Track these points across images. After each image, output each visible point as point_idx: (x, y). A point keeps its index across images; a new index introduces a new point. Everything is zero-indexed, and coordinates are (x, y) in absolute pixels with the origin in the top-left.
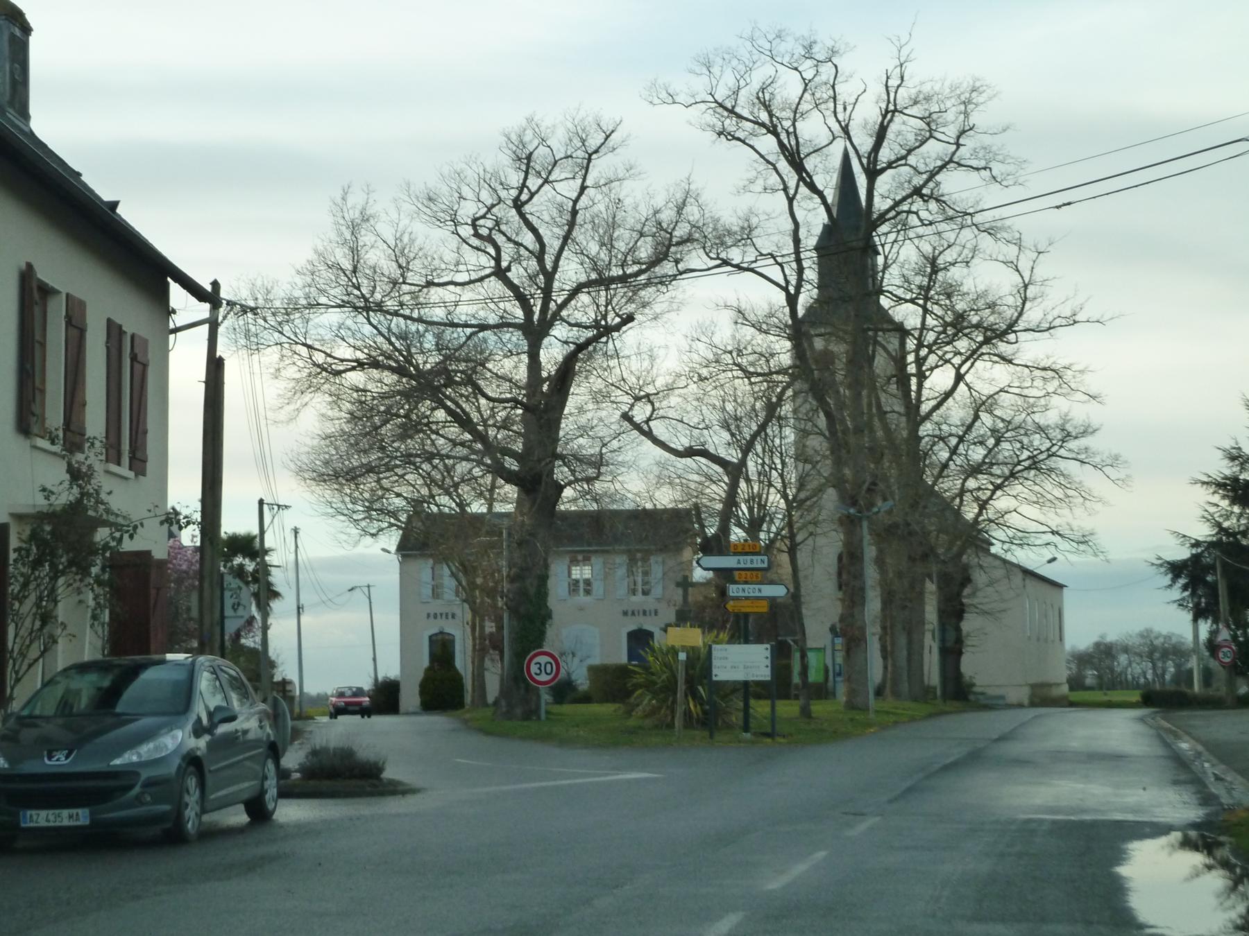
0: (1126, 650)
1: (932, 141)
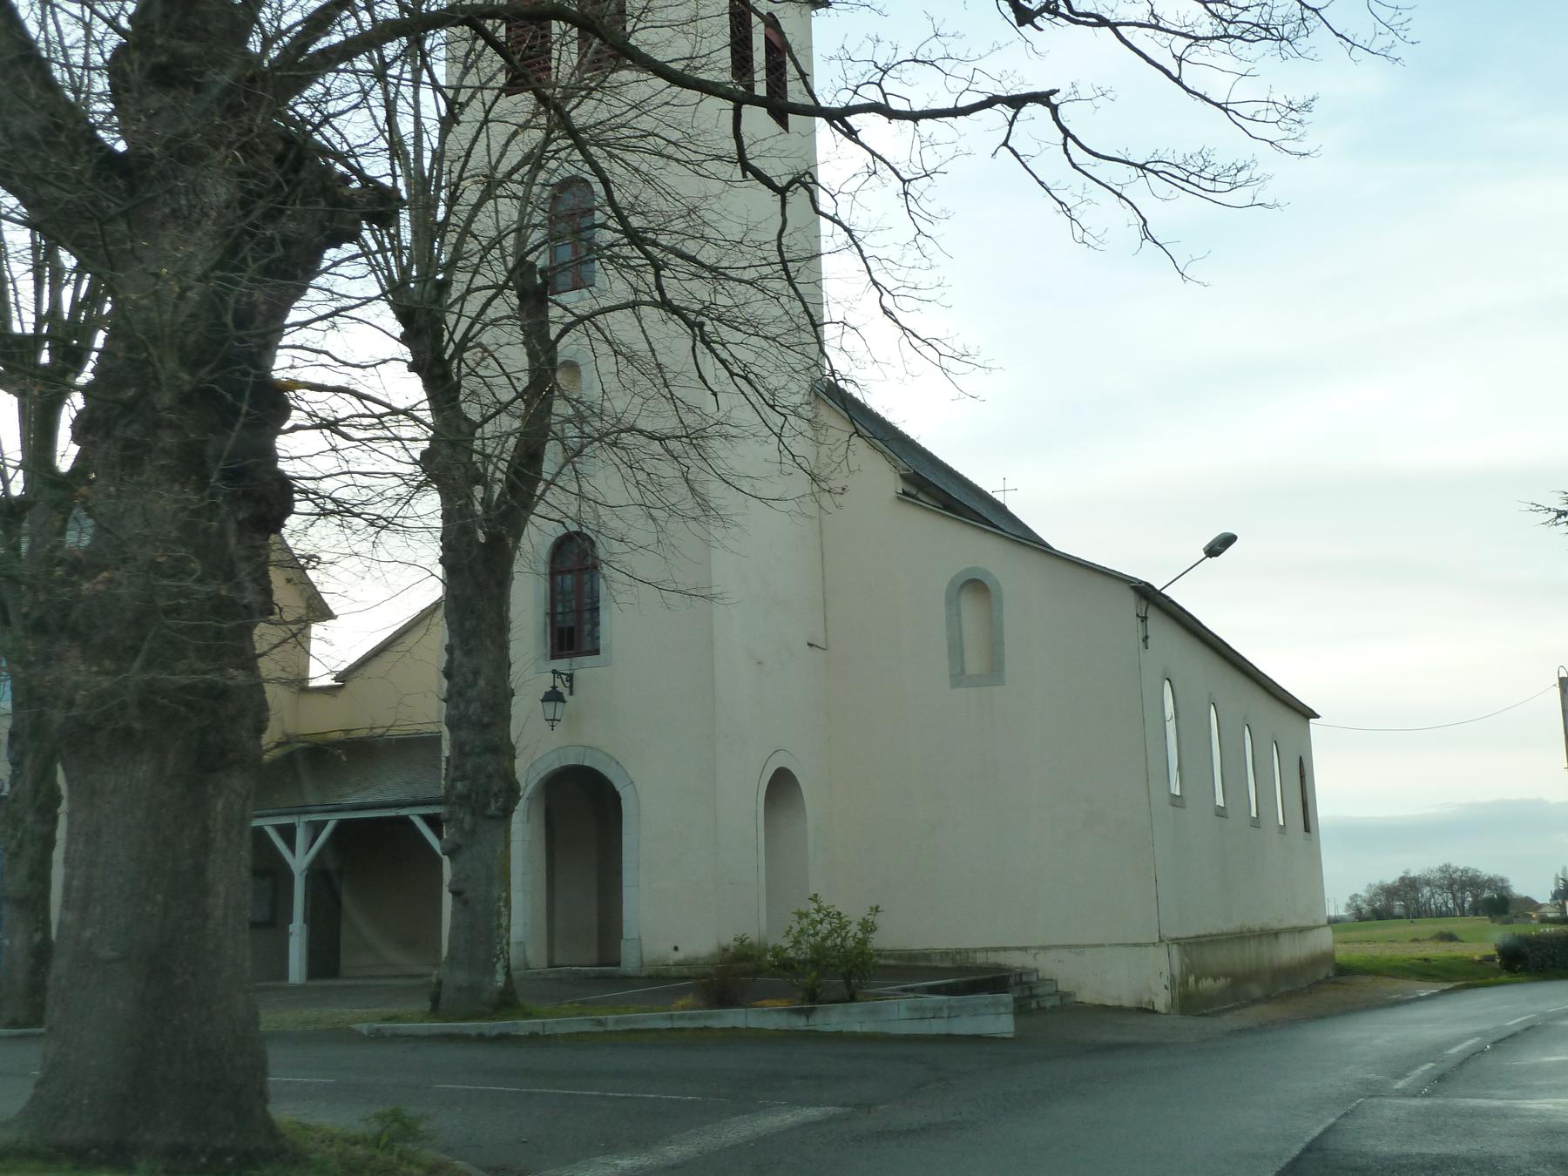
0: (1428, 883)
1: (770, 200)
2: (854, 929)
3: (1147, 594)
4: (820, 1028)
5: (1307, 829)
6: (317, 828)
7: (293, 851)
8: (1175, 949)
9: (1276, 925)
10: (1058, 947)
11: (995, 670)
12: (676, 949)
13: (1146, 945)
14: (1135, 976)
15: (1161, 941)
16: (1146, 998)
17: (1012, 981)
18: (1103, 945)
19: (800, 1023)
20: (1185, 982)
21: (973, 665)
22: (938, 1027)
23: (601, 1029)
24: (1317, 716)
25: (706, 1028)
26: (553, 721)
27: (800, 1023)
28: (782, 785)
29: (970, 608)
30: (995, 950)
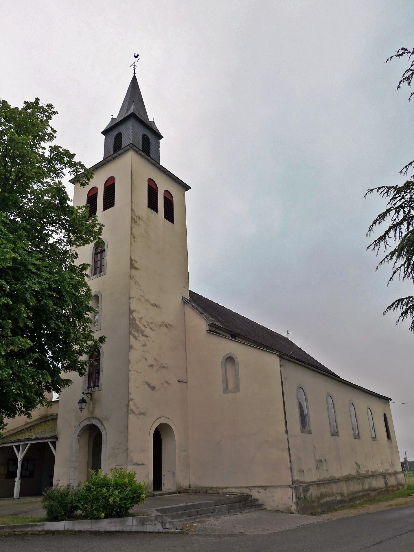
5: (389, 437)
7: (19, 452)
11: (237, 389)
21: (231, 386)
24: (391, 400)
26: (82, 409)
29: (229, 367)
30: (226, 488)
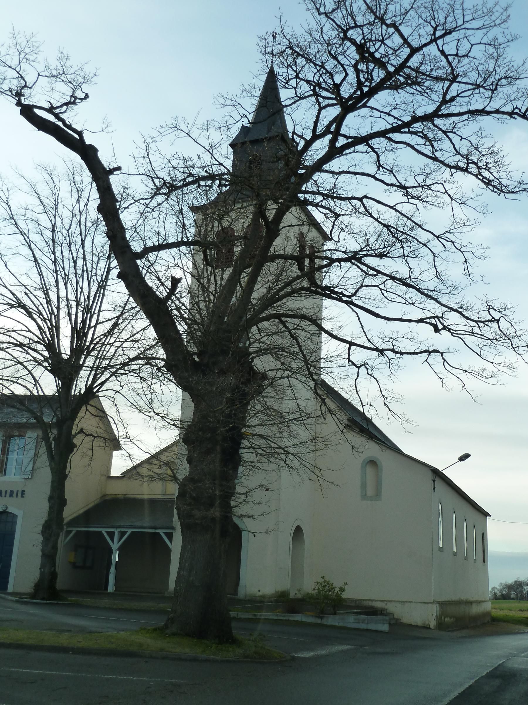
2: (337, 590)
3: (437, 474)
4: (325, 623)
5: (484, 561)
6: (122, 534)
7: (113, 541)
8: (438, 605)
9: (471, 599)
10: (395, 601)
11: (378, 495)
12: (259, 591)
13: (428, 603)
14: (424, 615)
15: (433, 602)
16: (427, 623)
17: (379, 612)
18: (412, 602)
19: (319, 621)
20: (440, 618)
22: (364, 626)
23: (255, 617)
25: (288, 620)
27: (319, 621)
28: (298, 531)
29: (370, 471)
30: (372, 600)
